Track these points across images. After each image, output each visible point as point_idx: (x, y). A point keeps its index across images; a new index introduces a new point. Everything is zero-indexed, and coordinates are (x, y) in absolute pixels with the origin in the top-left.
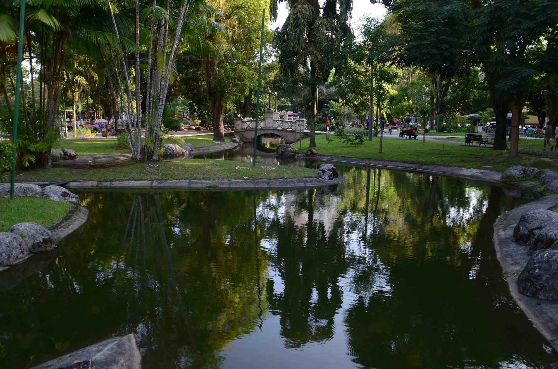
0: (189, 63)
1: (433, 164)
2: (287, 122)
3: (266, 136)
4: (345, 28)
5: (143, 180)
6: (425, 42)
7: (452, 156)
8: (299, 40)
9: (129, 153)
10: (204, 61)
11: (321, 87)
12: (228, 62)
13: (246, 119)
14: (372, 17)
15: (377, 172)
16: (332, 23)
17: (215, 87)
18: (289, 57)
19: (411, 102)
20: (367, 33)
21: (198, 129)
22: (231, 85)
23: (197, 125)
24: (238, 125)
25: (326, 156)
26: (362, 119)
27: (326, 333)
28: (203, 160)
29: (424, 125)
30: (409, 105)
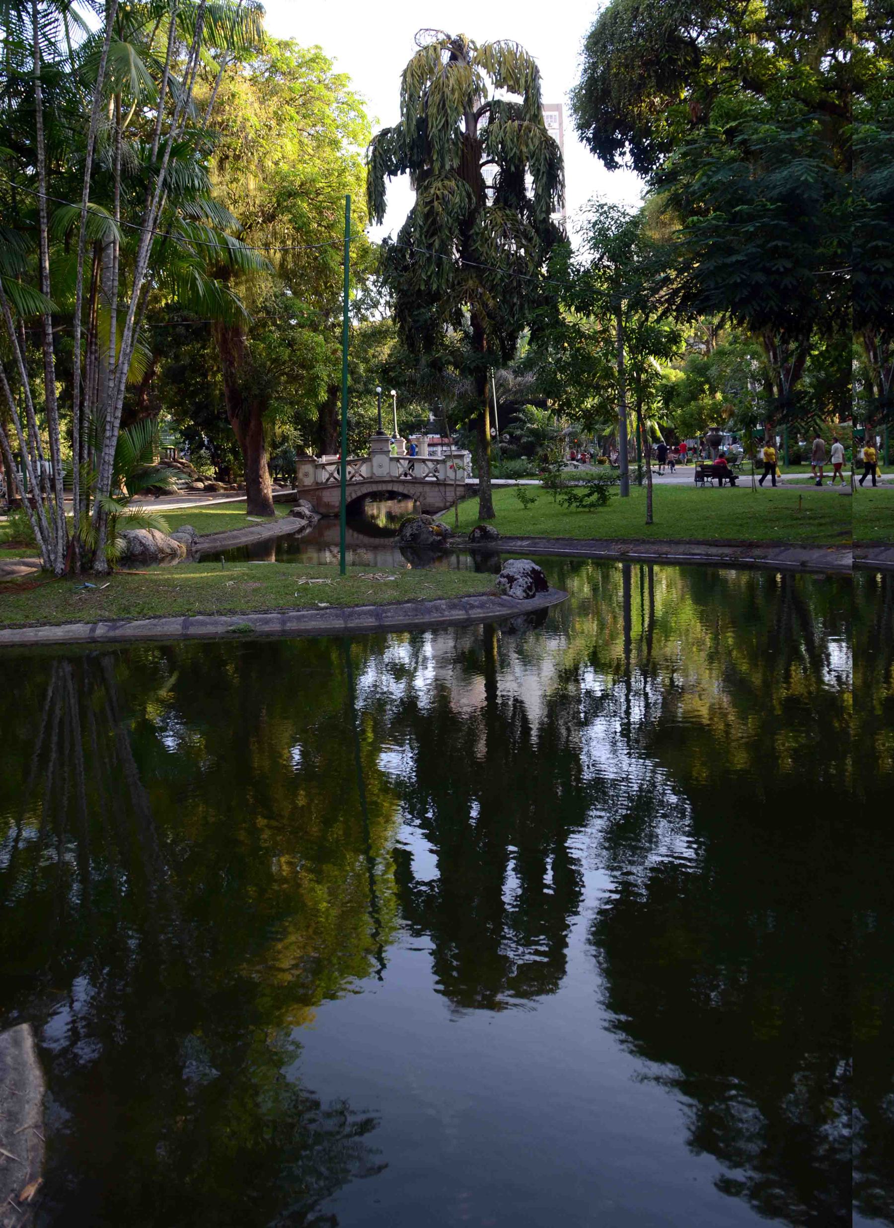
0: (181, 330)
1: (777, 544)
2: (424, 461)
3: (377, 496)
4: (547, 231)
5: (71, 623)
6: (734, 258)
7: (823, 521)
8: (439, 264)
9: (39, 556)
10: (216, 324)
11: (503, 372)
12: (274, 324)
13: (324, 459)
14: (610, 203)
15: (646, 569)
16: (515, 221)
17: (247, 387)
18: (419, 306)
19: (719, 396)
20: (600, 239)
21: (210, 489)
22: (283, 378)
23: (208, 479)
24: (306, 475)
25: (518, 538)
26: (606, 443)
27: (547, 975)
28: (220, 564)
29: (750, 451)
30: (714, 404)
